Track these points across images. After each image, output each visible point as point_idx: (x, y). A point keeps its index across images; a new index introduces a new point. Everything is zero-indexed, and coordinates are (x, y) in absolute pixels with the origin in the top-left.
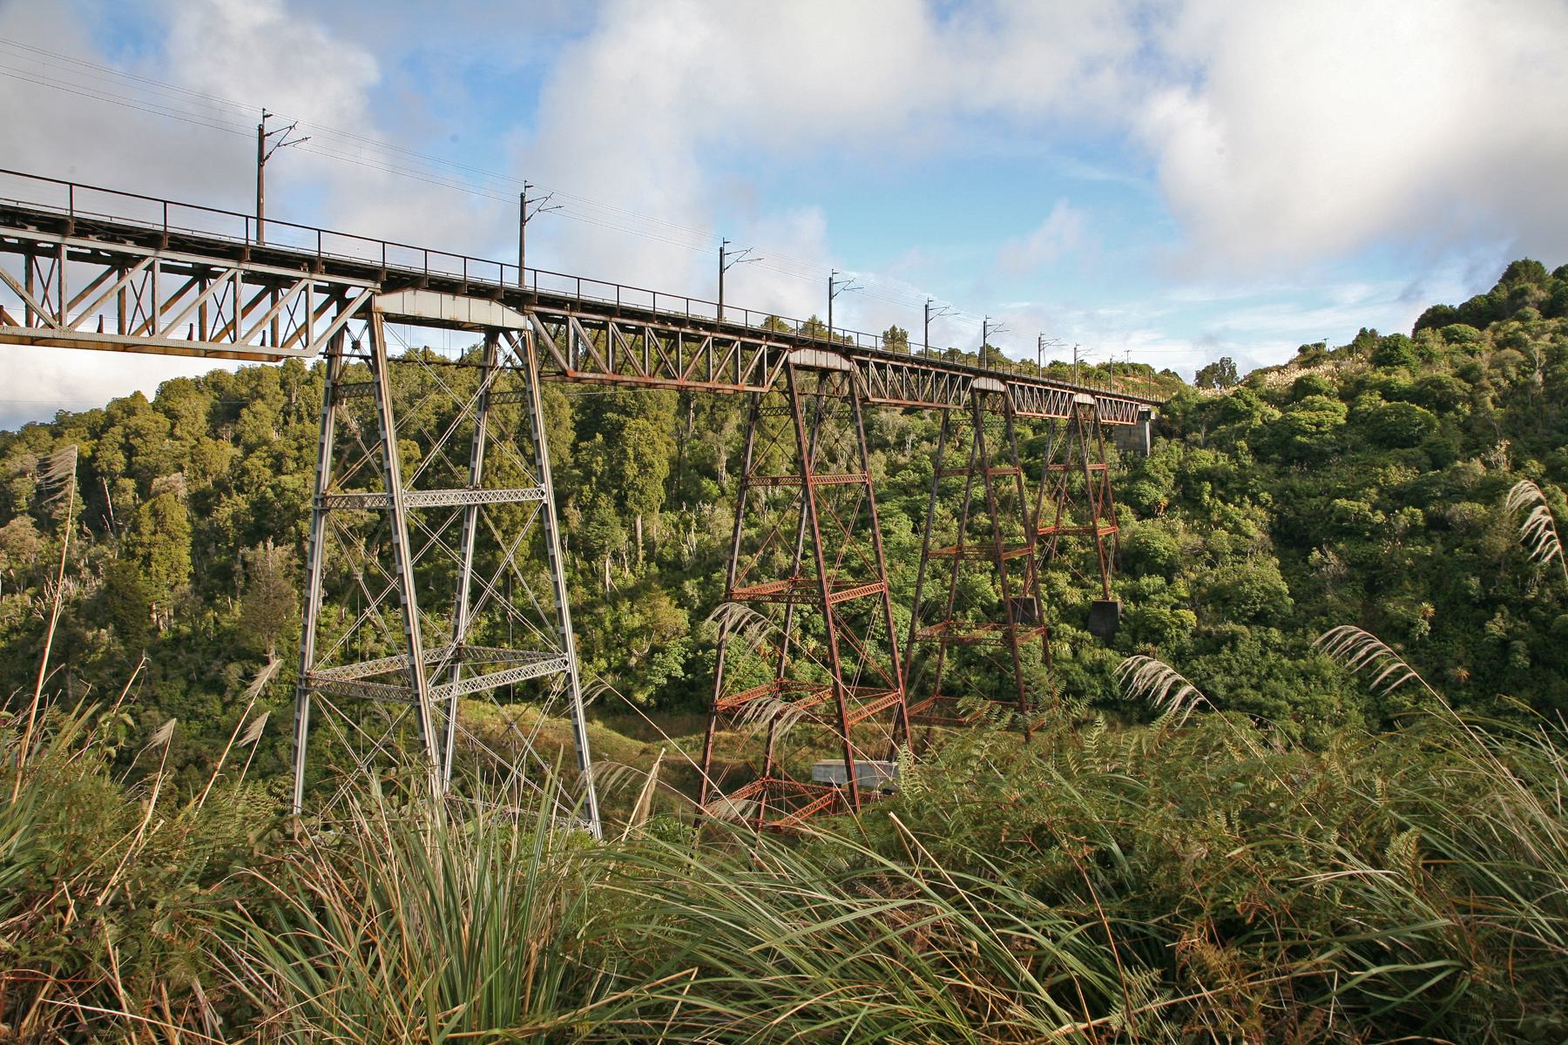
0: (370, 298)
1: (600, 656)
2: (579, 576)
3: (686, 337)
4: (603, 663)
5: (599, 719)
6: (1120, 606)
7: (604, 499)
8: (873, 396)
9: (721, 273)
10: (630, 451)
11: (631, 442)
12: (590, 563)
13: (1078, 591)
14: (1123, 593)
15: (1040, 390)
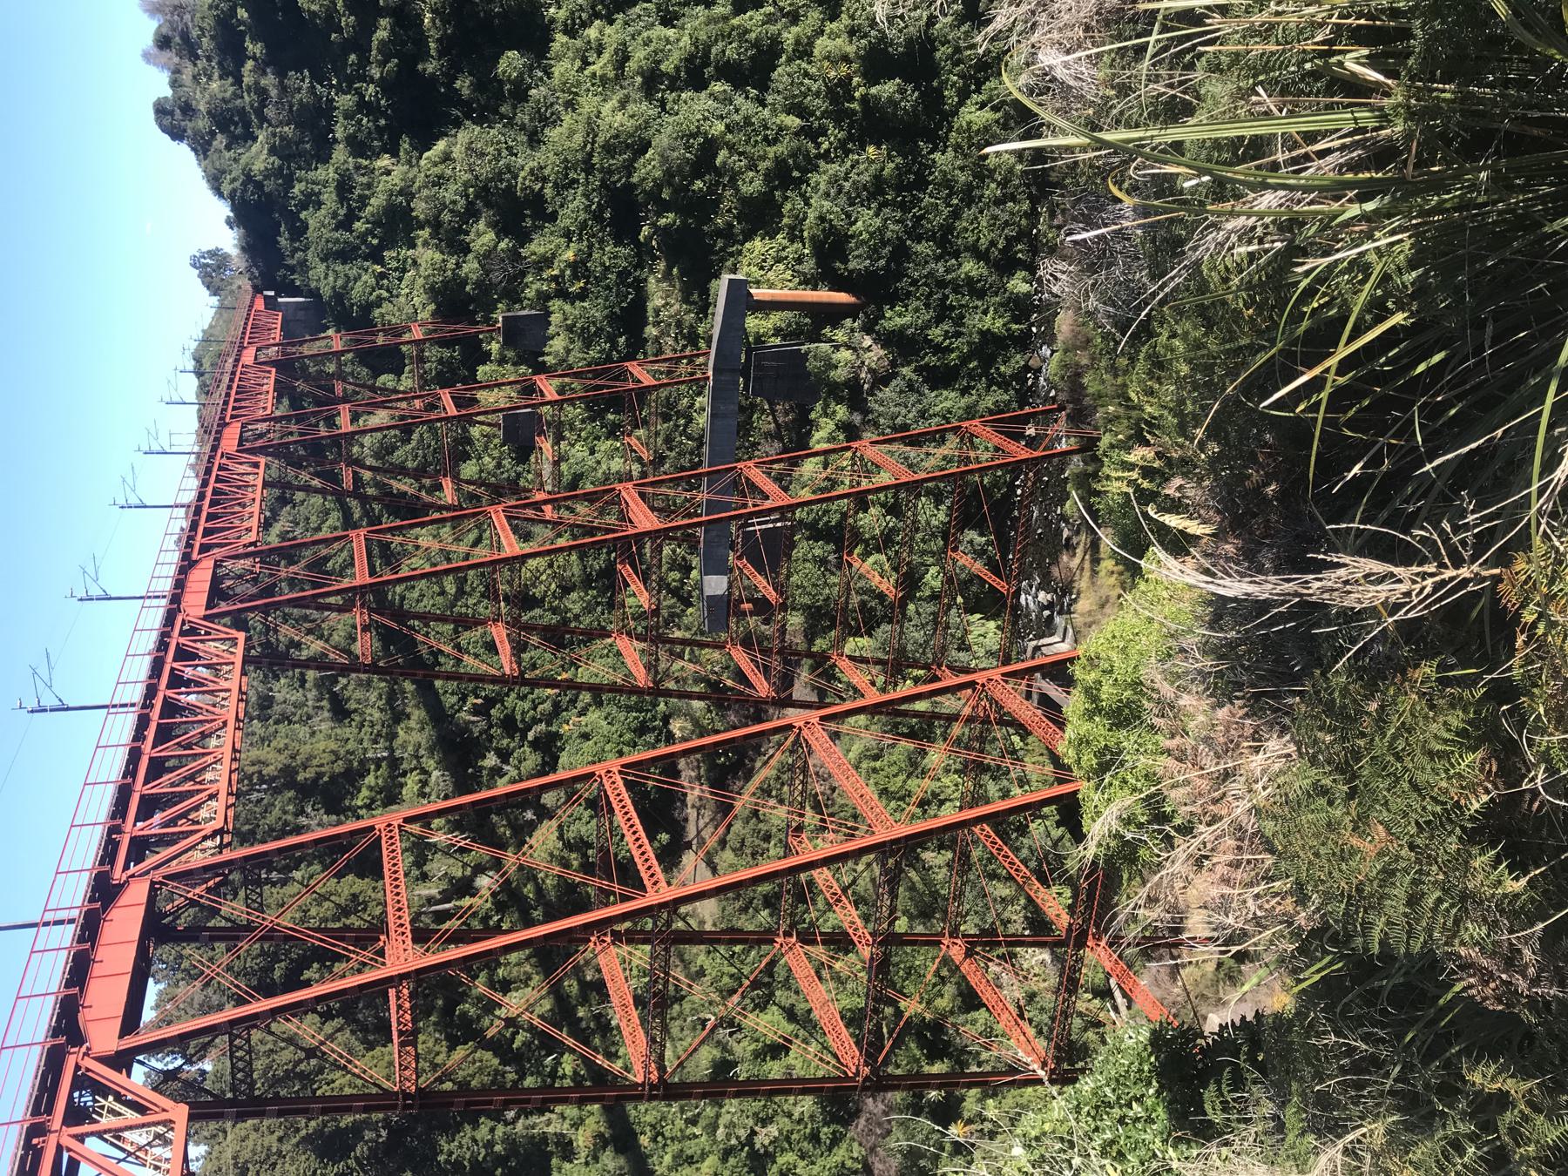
9: (68, 709)
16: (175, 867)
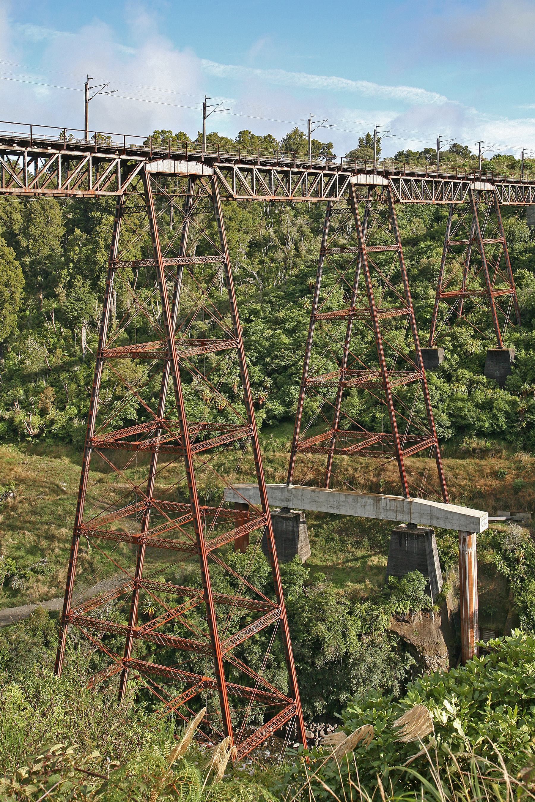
0: (143, 166)
1: (72, 404)
2: (62, 342)
3: (293, 173)
4: (74, 410)
5: (67, 456)
6: (512, 355)
7: (79, 281)
8: (403, 199)
10: (102, 242)
11: (102, 235)
12: (73, 331)
13: (478, 342)
14: (517, 344)
15: (521, 187)
16: (391, 193)
